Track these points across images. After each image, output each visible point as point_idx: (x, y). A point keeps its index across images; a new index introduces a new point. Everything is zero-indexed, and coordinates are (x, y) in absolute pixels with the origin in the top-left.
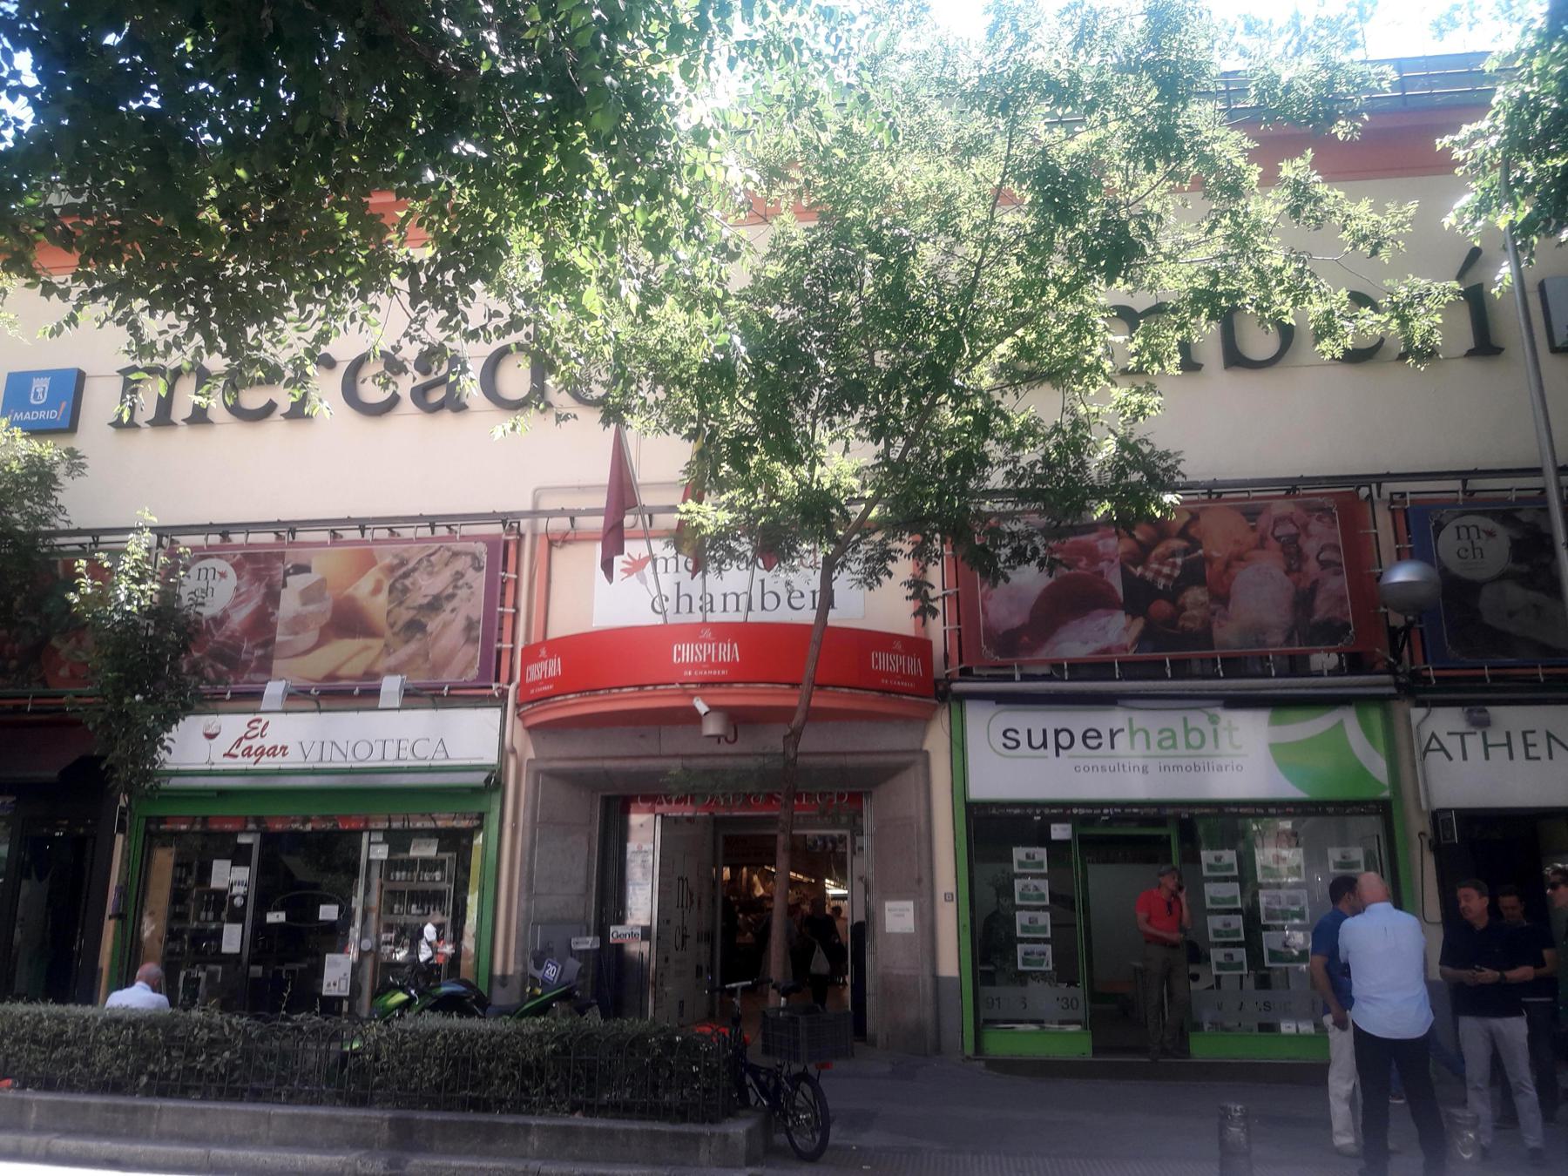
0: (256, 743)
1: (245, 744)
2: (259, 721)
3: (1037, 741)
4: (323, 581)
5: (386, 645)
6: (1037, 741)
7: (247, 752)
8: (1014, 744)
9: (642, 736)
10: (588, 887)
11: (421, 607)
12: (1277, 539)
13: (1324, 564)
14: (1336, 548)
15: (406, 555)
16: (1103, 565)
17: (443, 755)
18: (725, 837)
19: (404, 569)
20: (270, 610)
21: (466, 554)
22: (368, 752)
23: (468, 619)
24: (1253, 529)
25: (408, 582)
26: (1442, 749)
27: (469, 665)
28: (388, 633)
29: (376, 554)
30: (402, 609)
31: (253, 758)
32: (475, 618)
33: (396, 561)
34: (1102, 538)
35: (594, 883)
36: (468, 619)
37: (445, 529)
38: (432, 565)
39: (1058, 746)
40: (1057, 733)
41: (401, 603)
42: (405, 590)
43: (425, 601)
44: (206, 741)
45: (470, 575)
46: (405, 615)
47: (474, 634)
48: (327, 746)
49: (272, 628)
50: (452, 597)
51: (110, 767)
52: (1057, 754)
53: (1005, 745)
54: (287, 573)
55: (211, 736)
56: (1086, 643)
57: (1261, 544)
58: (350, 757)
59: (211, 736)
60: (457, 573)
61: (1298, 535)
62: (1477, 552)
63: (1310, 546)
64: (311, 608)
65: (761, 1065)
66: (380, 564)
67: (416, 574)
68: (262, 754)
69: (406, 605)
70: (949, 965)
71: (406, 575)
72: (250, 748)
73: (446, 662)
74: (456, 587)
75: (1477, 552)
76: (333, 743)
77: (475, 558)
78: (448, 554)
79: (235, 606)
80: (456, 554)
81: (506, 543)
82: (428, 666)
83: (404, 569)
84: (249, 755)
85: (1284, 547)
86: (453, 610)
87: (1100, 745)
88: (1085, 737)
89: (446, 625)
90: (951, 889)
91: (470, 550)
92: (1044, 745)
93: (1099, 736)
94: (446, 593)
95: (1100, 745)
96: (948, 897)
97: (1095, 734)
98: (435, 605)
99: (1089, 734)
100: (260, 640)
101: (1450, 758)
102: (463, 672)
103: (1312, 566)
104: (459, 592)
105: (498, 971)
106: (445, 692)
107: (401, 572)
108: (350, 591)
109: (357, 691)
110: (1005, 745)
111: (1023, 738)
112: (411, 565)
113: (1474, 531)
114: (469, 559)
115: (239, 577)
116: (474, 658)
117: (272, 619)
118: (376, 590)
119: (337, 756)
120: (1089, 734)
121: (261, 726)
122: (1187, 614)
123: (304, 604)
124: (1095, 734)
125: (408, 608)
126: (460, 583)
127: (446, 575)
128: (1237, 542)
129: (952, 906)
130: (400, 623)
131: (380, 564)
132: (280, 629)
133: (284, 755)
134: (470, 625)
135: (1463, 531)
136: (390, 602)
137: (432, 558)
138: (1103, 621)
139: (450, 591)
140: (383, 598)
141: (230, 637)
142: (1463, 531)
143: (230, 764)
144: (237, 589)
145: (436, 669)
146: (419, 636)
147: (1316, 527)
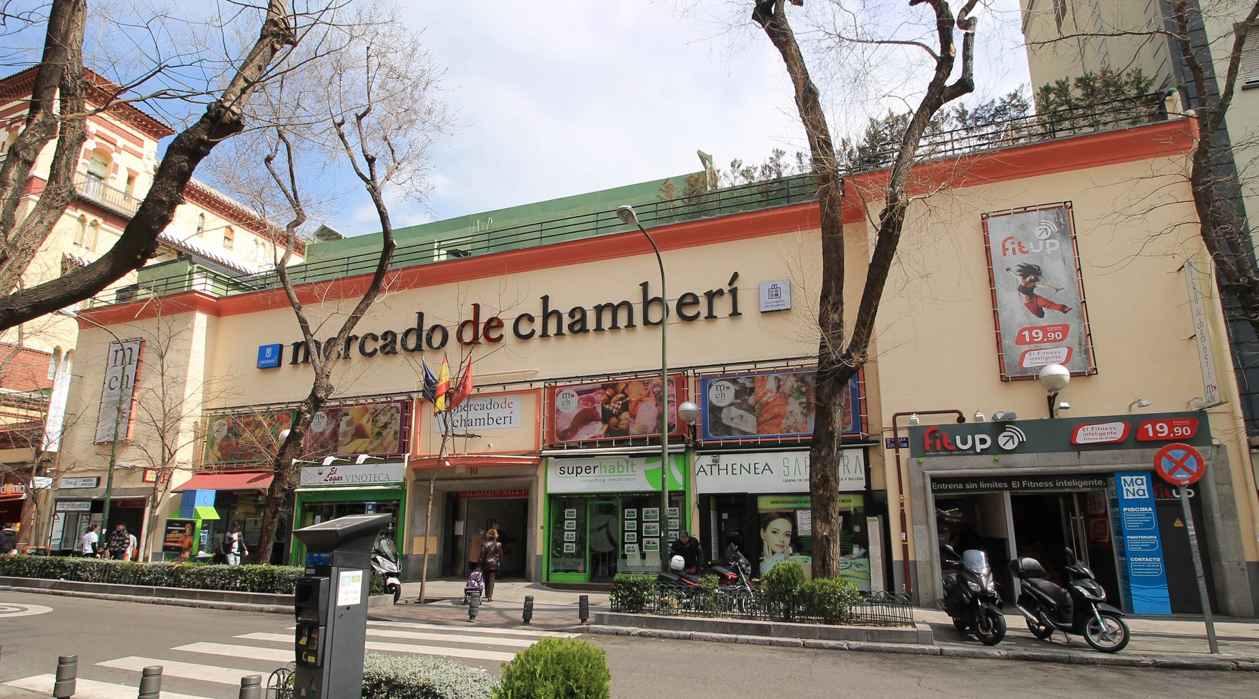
42: (377, 421)
55: (320, 474)
101: (248, 482)
127: (389, 415)
134: (396, 433)
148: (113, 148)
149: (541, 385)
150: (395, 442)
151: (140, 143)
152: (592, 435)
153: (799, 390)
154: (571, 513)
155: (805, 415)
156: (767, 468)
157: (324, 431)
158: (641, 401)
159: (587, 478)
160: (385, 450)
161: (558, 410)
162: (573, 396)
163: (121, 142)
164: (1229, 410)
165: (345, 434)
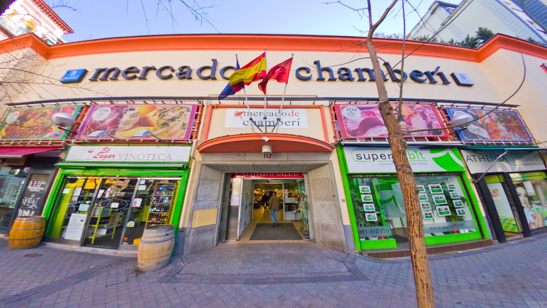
0: (104, 154)
1: (101, 154)
2: (107, 148)
3: (367, 157)
4: (138, 113)
5: (155, 129)
6: (367, 157)
7: (101, 157)
8: (360, 158)
9: (239, 155)
10: (219, 197)
11: (168, 120)
12: (419, 112)
13: (432, 118)
14: (433, 115)
15: (166, 107)
16: (377, 116)
17: (169, 159)
18: (282, 184)
19: (165, 110)
20: (119, 119)
21: (185, 108)
22: (143, 157)
23: (183, 123)
24: (413, 110)
25: (165, 114)
26: (470, 159)
27: (182, 135)
28: (156, 126)
29: (156, 107)
30: (162, 120)
31: (103, 158)
32: (185, 123)
33: (163, 109)
34: (375, 110)
35: (221, 197)
36: (183, 123)
37: (180, 102)
38: (174, 110)
39: (373, 158)
40: (373, 155)
41: (162, 118)
42: (164, 115)
43: (170, 118)
44: (88, 153)
45: (186, 113)
46: (163, 121)
47: (184, 127)
48: (129, 155)
49: (118, 124)
50: (179, 117)
51: (323, 239)
52: (374, 161)
53: (357, 158)
54: (127, 110)
55: (90, 152)
56: (376, 133)
57: (415, 113)
58: (136, 159)
59: (90, 152)
60: (182, 112)
61: (423, 112)
62: (353, 113)
63: (427, 114)
64: (132, 119)
65: (70, 184)
66: (157, 109)
67: (168, 112)
68: (106, 157)
69: (164, 119)
70: (347, 221)
71: (165, 112)
72: (102, 155)
73: (175, 133)
74: (181, 115)
75: (353, 113)
76: (131, 155)
77: (188, 108)
78: (179, 107)
79: (108, 118)
80: (182, 108)
81: (198, 107)
82: (168, 134)
83: (165, 110)
84: (101, 157)
85: (421, 114)
86: (179, 121)
87: (386, 158)
88: (381, 156)
89: (176, 124)
90: (344, 198)
91: (187, 107)
92: (369, 158)
93: (385, 156)
94: (177, 117)
95: (386, 158)
96: (343, 201)
97: (384, 156)
98: (173, 119)
99: (382, 155)
100: (113, 126)
101: (473, 161)
102: (180, 136)
103: (429, 118)
104: (182, 117)
105: (181, 226)
106: (172, 142)
107: (164, 111)
108: (146, 115)
109: (157, 141)
110: (357, 158)
111: (363, 156)
112: (167, 110)
113: (351, 110)
114: (186, 109)
115: (112, 111)
116: (184, 133)
117: (119, 121)
118: (155, 115)
119: (133, 159)
120: (382, 155)
121: (107, 149)
122: (402, 127)
123: (131, 118)
124: (384, 156)
125: (164, 120)
126: (182, 114)
127: (178, 112)
128: (409, 112)
129: (345, 203)
130: (161, 123)
131: (157, 109)
132: (121, 124)
133: (113, 158)
134: (184, 125)
135: (349, 109)
136: (158, 118)
137: (174, 108)
138: (380, 128)
139: (179, 116)
140: (156, 117)
141: (104, 126)
142: (349, 109)
143: (95, 160)
144: (110, 114)
145: (170, 135)
146: (166, 127)
147: (427, 110)
148: (39, 24)
149: (326, 103)
150: (183, 131)
151: (55, 29)
152: (380, 134)
153: (499, 119)
154: (365, 189)
155: (508, 131)
156: (169, 157)
157: (105, 120)
158: (411, 116)
159: (382, 163)
160: (170, 135)
161: (345, 118)
162: (356, 110)
163: (43, 23)
164: (148, 155)
165: (127, 123)
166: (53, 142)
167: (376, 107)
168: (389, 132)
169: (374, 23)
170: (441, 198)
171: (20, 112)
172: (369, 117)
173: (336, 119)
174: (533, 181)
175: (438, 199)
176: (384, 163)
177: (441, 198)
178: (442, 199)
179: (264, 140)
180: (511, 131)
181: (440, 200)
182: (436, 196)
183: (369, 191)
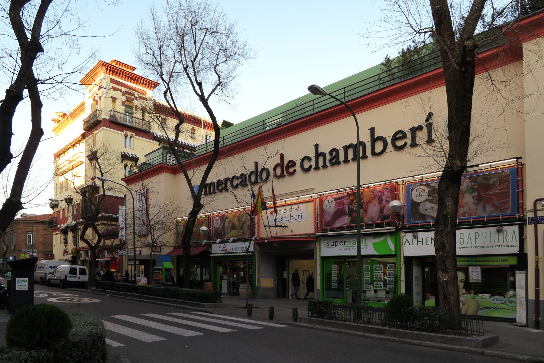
26: (409, 243)
39: (336, 245)
40: (336, 242)
101: (410, 245)
152: (343, 223)
166: (501, 167)
167: (346, 196)
168: (439, 211)
169: (331, 97)
170: (379, 276)
171: (183, 223)
172: (339, 207)
173: (396, 188)
174: (482, 267)
175: (378, 276)
176: (342, 248)
177: (379, 276)
178: (380, 277)
179: (18, 219)
180: (481, 204)
181: (378, 277)
182: (377, 274)
183: (382, 288)
